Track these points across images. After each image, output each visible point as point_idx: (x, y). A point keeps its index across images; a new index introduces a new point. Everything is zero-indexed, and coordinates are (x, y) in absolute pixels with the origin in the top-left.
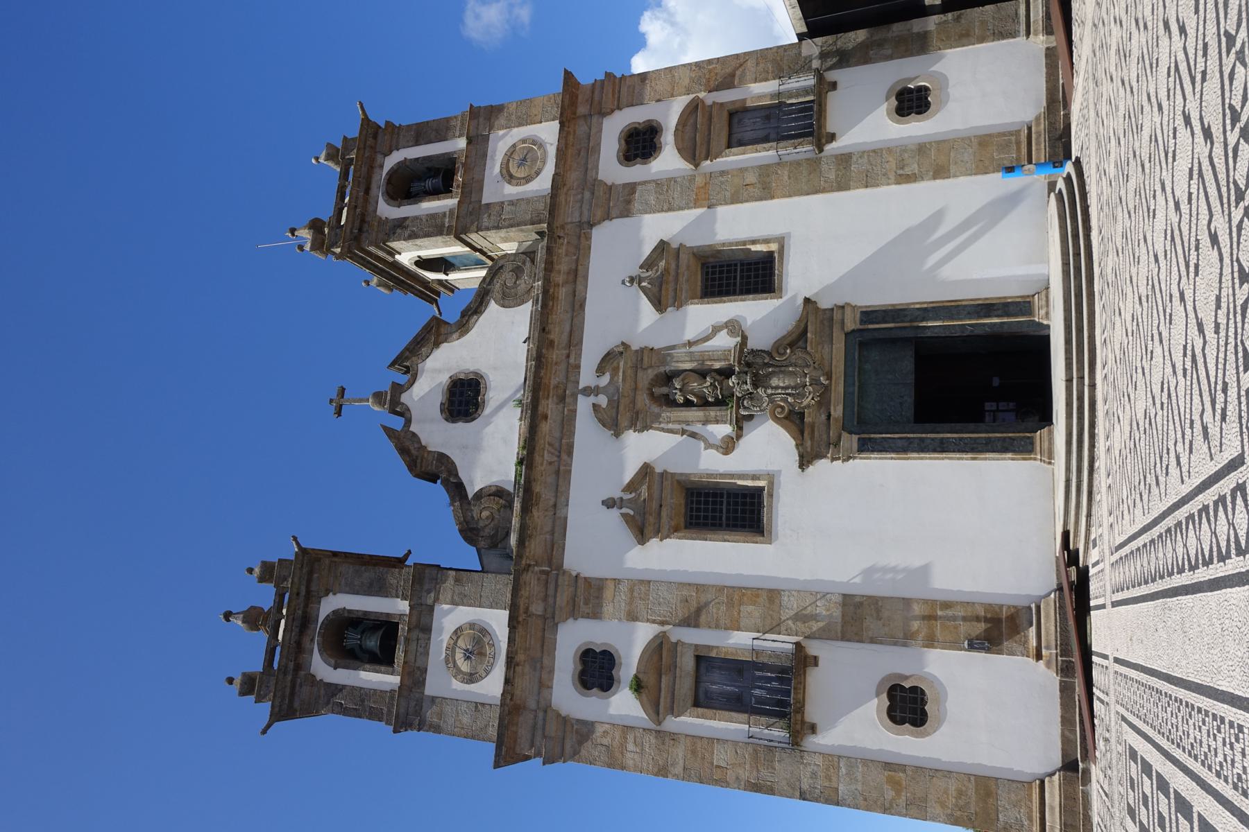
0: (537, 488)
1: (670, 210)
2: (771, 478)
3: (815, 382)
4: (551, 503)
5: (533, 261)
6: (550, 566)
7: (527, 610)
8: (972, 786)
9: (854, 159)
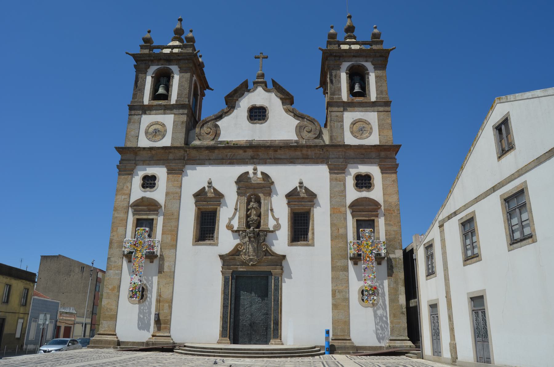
0: (216, 151)
1: (331, 197)
2: (217, 245)
3: (251, 260)
4: (211, 158)
5: (315, 138)
6: (188, 160)
7: (170, 152)
8: (114, 313)
9: (345, 273)
